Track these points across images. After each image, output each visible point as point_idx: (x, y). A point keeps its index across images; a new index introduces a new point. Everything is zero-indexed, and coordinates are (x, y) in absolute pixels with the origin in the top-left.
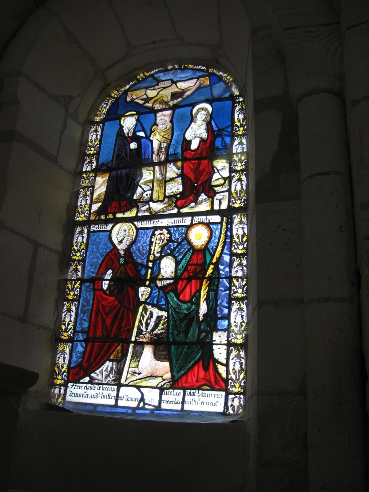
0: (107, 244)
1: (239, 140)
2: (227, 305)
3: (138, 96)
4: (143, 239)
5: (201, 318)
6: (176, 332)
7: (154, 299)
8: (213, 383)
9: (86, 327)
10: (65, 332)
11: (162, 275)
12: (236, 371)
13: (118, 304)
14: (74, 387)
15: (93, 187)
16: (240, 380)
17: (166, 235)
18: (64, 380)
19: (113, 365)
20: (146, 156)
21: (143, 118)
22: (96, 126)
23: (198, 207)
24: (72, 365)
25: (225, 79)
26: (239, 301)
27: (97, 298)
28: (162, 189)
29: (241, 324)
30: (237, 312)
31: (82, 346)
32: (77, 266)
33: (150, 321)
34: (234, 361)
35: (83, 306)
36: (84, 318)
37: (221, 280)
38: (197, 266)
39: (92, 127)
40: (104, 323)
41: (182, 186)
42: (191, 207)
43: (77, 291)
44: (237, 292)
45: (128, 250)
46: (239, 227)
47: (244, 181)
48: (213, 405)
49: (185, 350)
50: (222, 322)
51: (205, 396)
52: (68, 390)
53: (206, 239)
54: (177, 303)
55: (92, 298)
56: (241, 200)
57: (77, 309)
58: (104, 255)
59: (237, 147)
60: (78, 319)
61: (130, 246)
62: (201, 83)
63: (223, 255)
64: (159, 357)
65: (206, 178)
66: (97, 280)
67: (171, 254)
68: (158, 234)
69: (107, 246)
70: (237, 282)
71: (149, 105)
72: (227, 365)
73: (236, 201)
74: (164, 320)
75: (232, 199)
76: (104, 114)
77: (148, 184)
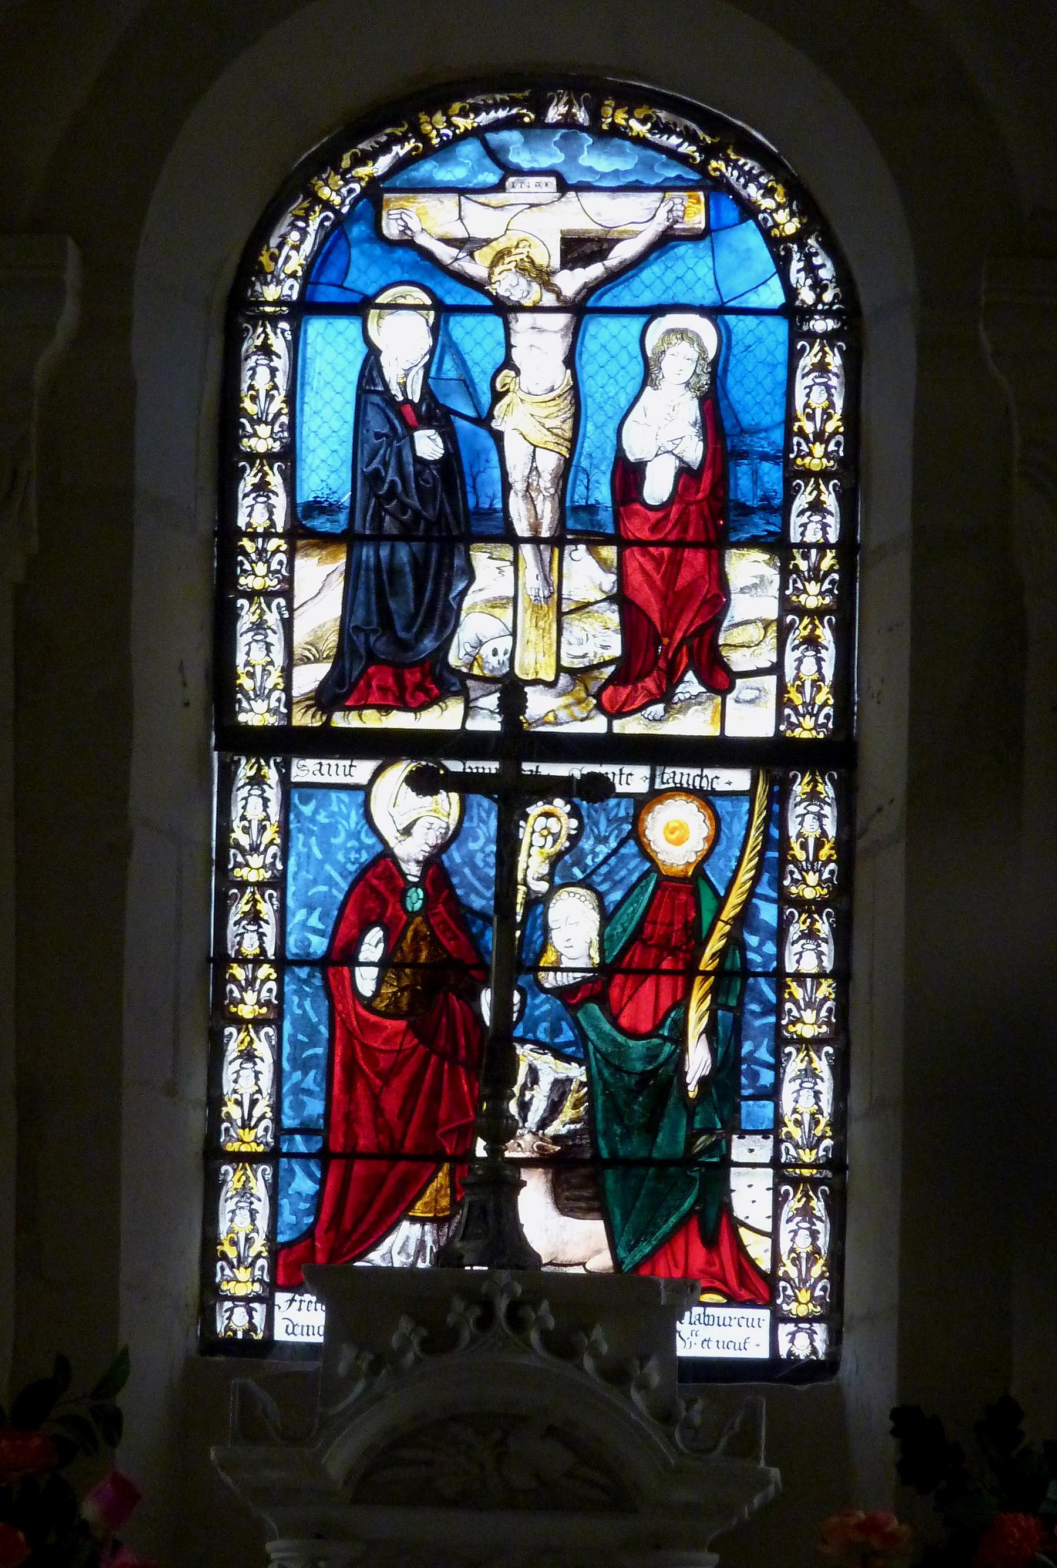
0: (360, 832)
1: (810, 494)
2: (772, 1060)
3: (425, 219)
4: (484, 828)
5: (692, 1091)
6: (619, 1131)
7: (536, 1025)
8: (733, 1281)
9: (319, 1116)
10: (243, 1127)
11: (557, 951)
12: (798, 1254)
13: (417, 1046)
14: (296, 1305)
15: (287, 593)
16: (812, 1280)
17: (564, 818)
18: (261, 1281)
19: (423, 1235)
20: (481, 500)
21: (461, 327)
22: (265, 327)
23: (676, 721)
24: (281, 1238)
25: (765, 220)
26: (807, 1049)
27: (343, 1021)
28: (547, 636)
29: (814, 1118)
30: (802, 1082)
31: (310, 1175)
32: (255, 901)
33: (533, 1097)
34: (792, 1226)
35: (295, 1043)
36: (303, 1086)
37: (751, 980)
38: (664, 929)
39: (247, 330)
40: (377, 1110)
41: (619, 637)
42: (650, 717)
43: (270, 991)
44: (799, 1020)
45: (434, 865)
46: (808, 813)
47: (827, 649)
48: (737, 1347)
49: (648, 1184)
50: (414, 174)
51: (711, 1322)
52: (278, 1314)
53: (702, 846)
54: (614, 1040)
55: (325, 1019)
56: (817, 716)
57: (277, 1051)
58: (350, 873)
59: (804, 519)
60: (285, 1090)
61: (442, 848)
62: (675, 214)
63: (755, 901)
64: (571, 1204)
65: (699, 622)
66: (342, 955)
67: (586, 883)
68: (540, 815)
69: (358, 839)
70: (800, 990)
71: (477, 269)
72: (774, 1236)
73: (801, 719)
74: (578, 1091)
75: (787, 711)
76: (293, 275)
77: (497, 612)
